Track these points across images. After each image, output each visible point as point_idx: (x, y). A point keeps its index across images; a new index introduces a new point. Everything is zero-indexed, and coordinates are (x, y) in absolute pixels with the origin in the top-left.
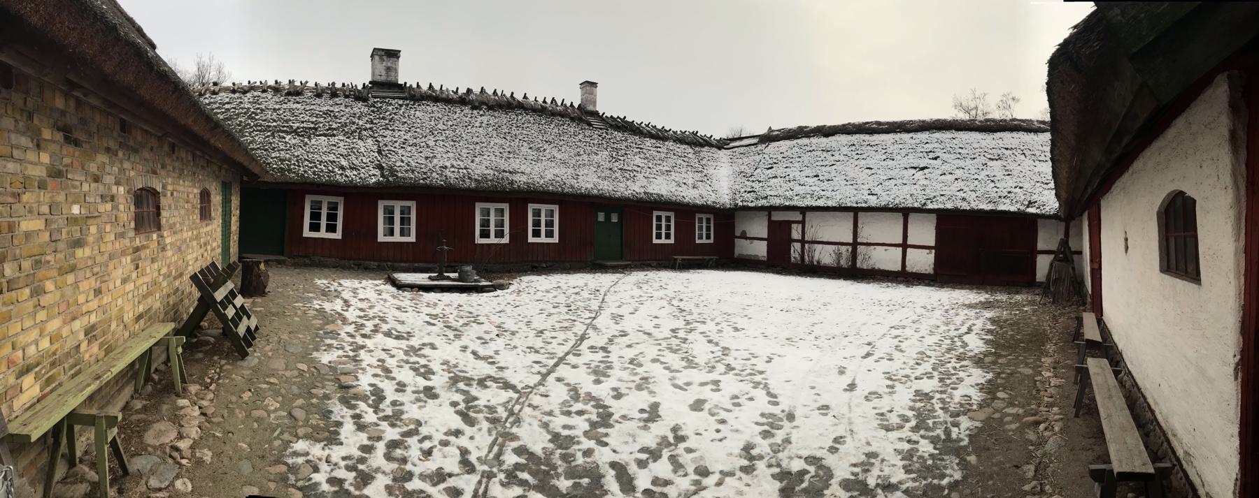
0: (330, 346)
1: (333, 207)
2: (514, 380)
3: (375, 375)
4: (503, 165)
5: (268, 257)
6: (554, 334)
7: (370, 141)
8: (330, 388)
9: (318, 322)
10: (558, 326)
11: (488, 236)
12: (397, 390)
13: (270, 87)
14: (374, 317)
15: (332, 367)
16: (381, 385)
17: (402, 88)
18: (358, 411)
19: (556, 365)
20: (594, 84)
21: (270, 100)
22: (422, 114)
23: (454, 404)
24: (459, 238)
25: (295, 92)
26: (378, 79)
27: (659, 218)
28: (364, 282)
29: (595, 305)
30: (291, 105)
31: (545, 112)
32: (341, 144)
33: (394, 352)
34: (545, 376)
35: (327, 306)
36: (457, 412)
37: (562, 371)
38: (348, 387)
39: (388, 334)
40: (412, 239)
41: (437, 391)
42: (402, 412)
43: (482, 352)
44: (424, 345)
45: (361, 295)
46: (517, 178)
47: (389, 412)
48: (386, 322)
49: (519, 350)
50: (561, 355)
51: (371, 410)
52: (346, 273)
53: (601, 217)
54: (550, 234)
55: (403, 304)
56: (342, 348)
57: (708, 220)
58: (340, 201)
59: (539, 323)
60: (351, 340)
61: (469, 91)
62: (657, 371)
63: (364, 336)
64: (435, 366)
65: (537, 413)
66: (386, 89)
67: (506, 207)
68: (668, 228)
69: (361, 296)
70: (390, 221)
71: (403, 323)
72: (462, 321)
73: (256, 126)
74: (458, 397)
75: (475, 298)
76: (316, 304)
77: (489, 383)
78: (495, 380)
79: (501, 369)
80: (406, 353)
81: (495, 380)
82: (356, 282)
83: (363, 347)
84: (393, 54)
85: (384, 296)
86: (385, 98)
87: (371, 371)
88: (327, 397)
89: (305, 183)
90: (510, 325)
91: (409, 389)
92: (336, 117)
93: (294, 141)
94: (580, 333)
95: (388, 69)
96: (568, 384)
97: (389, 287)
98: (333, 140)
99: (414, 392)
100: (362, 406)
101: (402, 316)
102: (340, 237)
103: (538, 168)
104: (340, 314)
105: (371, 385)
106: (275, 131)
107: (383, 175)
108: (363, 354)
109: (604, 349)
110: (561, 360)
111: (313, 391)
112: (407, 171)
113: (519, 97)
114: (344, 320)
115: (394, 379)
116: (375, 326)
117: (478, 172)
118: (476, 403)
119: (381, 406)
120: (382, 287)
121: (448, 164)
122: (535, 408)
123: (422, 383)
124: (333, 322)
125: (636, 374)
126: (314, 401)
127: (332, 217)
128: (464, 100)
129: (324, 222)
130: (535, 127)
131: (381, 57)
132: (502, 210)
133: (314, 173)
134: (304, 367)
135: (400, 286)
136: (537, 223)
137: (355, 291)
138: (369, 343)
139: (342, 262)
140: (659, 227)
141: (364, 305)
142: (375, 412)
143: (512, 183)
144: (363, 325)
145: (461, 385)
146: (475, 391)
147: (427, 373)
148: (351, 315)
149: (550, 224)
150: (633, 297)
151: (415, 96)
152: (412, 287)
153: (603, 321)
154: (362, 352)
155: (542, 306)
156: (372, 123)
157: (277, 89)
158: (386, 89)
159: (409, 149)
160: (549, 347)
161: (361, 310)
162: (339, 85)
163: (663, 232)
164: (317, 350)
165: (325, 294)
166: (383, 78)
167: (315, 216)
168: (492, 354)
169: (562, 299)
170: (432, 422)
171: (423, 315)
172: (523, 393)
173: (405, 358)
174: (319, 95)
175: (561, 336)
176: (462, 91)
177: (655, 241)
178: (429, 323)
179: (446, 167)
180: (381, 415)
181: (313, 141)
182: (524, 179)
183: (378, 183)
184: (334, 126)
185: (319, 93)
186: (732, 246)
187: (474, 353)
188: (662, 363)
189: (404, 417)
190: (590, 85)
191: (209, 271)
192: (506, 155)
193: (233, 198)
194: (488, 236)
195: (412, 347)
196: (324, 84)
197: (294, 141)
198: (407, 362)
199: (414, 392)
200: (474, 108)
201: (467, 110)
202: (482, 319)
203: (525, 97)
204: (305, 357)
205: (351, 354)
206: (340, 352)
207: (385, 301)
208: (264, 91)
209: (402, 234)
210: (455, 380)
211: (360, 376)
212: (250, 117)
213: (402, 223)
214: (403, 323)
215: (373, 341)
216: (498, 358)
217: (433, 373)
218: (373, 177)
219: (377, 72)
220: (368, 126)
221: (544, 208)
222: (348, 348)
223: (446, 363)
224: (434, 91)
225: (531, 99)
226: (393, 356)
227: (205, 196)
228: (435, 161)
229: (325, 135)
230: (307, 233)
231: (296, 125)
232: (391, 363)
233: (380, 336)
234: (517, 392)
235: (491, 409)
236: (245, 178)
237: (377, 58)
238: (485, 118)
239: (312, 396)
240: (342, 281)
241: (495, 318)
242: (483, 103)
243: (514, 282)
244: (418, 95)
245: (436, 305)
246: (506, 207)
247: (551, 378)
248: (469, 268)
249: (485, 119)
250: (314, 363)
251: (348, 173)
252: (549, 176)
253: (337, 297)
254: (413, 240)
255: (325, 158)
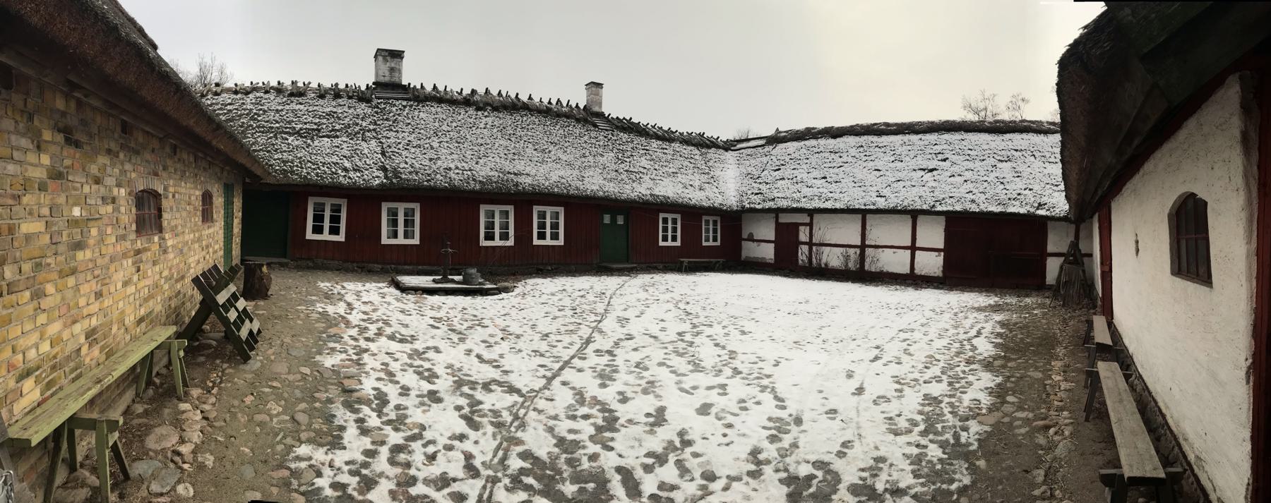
0: (333, 349)
1: (336, 209)
2: (519, 384)
3: (379, 379)
4: (508, 166)
5: (270, 260)
6: (559, 338)
7: (373, 142)
8: (333, 392)
9: (321, 326)
10: (563, 329)
11: (492, 239)
12: (401, 394)
13: (272, 88)
14: (378, 320)
15: (335, 371)
16: (384, 389)
17: (405, 88)
18: (361, 415)
19: (561, 369)
20: (599, 85)
21: (273, 101)
22: (426, 115)
23: (459, 408)
24: (463, 240)
25: (298, 93)
26: (382, 79)
27: (665, 221)
28: (368, 285)
29: (600, 308)
30: (294, 106)
31: (550, 113)
32: (345, 146)
33: (398, 355)
34: (550, 380)
35: (331, 309)
36: (462, 417)
37: (568, 374)
38: (352, 391)
39: (392, 337)
40: (416, 241)
41: (441, 395)
42: (406, 417)
43: (486, 356)
44: (428, 348)
45: (364, 298)
46: (521, 179)
47: (393, 416)
48: (390, 326)
49: (524, 354)
50: (567, 358)
51: (374, 414)
52: (349, 275)
53: (607, 219)
54: (555, 236)
55: (407, 307)
56: (346, 352)
57: (715, 223)
58: (343, 203)
59: (544, 326)
60: (354, 343)
61: (474, 92)
62: (663, 374)
63: (367, 339)
64: (439, 370)
65: (542, 417)
66: (390, 90)
67: (510, 209)
68: (674, 230)
69: (364, 299)
70: (394, 223)
71: (407, 326)
72: (466, 325)
73: (258, 127)
74: (463, 401)
75: (479, 301)
76: (319, 307)
77: (493, 387)
78: (500, 384)
79: (506, 372)
80: (410, 356)
81: (500, 384)
82: (360, 284)
83: (366, 351)
84: (397, 55)
85: (388, 299)
86: (389, 99)
87: (375, 375)
88: (330, 401)
89: (308, 185)
90: (515, 328)
91: (413, 393)
92: (339, 118)
93: (297, 143)
94: (585, 336)
95: (392, 70)
96: (573, 388)
97: (393, 290)
98: (337, 142)
99: (418, 396)
100: (366, 410)
101: (406, 319)
102: (343, 240)
103: (543, 169)
104: (343, 318)
105: (375, 389)
106: (277, 133)
107: (386, 177)
108: (366, 358)
109: (610, 353)
110: (567, 363)
111: (316, 395)
112: (410, 173)
113: (524, 98)
114: (348, 324)
115: (398, 382)
116: (379, 329)
117: (483, 173)
118: (481, 407)
119: (385, 410)
120: (386, 290)
121: (452, 166)
122: (540, 412)
123: (426, 387)
124: (336, 325)
125: (642, 378)
126: (317, 405)
127: (335, 219)
128: (468, 101)
129: (327, 224)
130: (540, 128)
131: (384, 57)
132: (507, 213)
133: (317, 175)
134: (307, 371)
135: (404, 289)
136: (542, 226)
137: (358, 294)
138: (372, 346)
139: (346, 265)
140: (665, 229)
141: (368, 308)
142: (379, 416)
143: (517, 185)
144: (366, 328)
145: (466, 389)
146: (479, 395)
147: (431, 377)
148: (355, 318)
149: (555, 226)
150: (639, 300)
151: (419, 97)
152: (415, 290)
153: (609, 324)
154: (365, 356)
155: (547, 309)
156: (375, 124)
157: (279, 90)
158: (390, 90)
159: (413, 150)
160: (555, 350)
161: (365, 313)
162: (342, 86)
163: (670, 234)
164: (320, 354)
165: (328, 297)
166: (387, 79)
167: (318, 218)
168: (497, 357)
169: (567, 302)
170: (436, 426)
171: (427, 319)
172: (528, 397)
173: (409, 361)
174: (322, 96)
175: (567, 339)
176: (467, 92)
177: (661, 243)
178: (433, 326)
179: (450, 169)
180: (385, 419)
181: (316, 143)
182: (529, 180)
183: (382, 185)
184: (338, 127)
185: (322, 94)
186: (739, 249)
187: (478, 356)
188: (668, 367)
189: (408, 421)
190: (595, 86)
191: (211, 274)
192: (510, 156)
193: (235, 200)
194: (492, 239)
195: (416, 350)
196: (327, 85)
197: (297, 143)
198: (411, 366)
199: (418, 396)
200: (478, 109)
201: (471, 111)
202: (486, 322)
203: (530, 98)
204: (308, 360)
205: (355, 357)
206: (344, 356)
207: (389, 304)
208: (267, 92)
209: (406, 236)
210: (459, 384)
211: (363, 380)
212: (253, 119)
213: (406, 226)
214: (407, 326)
215: (376, 344)
216: (502, 362)
217: (438, 377)
218: (376, 178)
219: (381, 73)
220: (372, 127)
221: (549, 210)
222: (351, 352)
223: (450, 366)
224: (438, 92)
225: (536, 100)
226: (397, 360)
227: (207, 198)
228: (439, 163)
229: (328, 137)
230: (310, 235)
231: (299, 126)
232: (395, 367)
233: (384, 339)
234: (522, 396)
235: (496, 413)
236: (247, 180)
237: (380, 58)
238: (490, 119)
239: (315, 400)
240: (345, 284)
241: (499, 322)
242: (488, 104)
243: (519, 285)
244: (422, 96)
245: (440, 308)
246: (510, 209)
247: (556, 382)
248: (473, 271)
249: (489, 120)
250: (317, 367)
251: (352, 174)
252: (554, 177)
253: (340, 300)
254: (417, 242)
255: (328, 160)
